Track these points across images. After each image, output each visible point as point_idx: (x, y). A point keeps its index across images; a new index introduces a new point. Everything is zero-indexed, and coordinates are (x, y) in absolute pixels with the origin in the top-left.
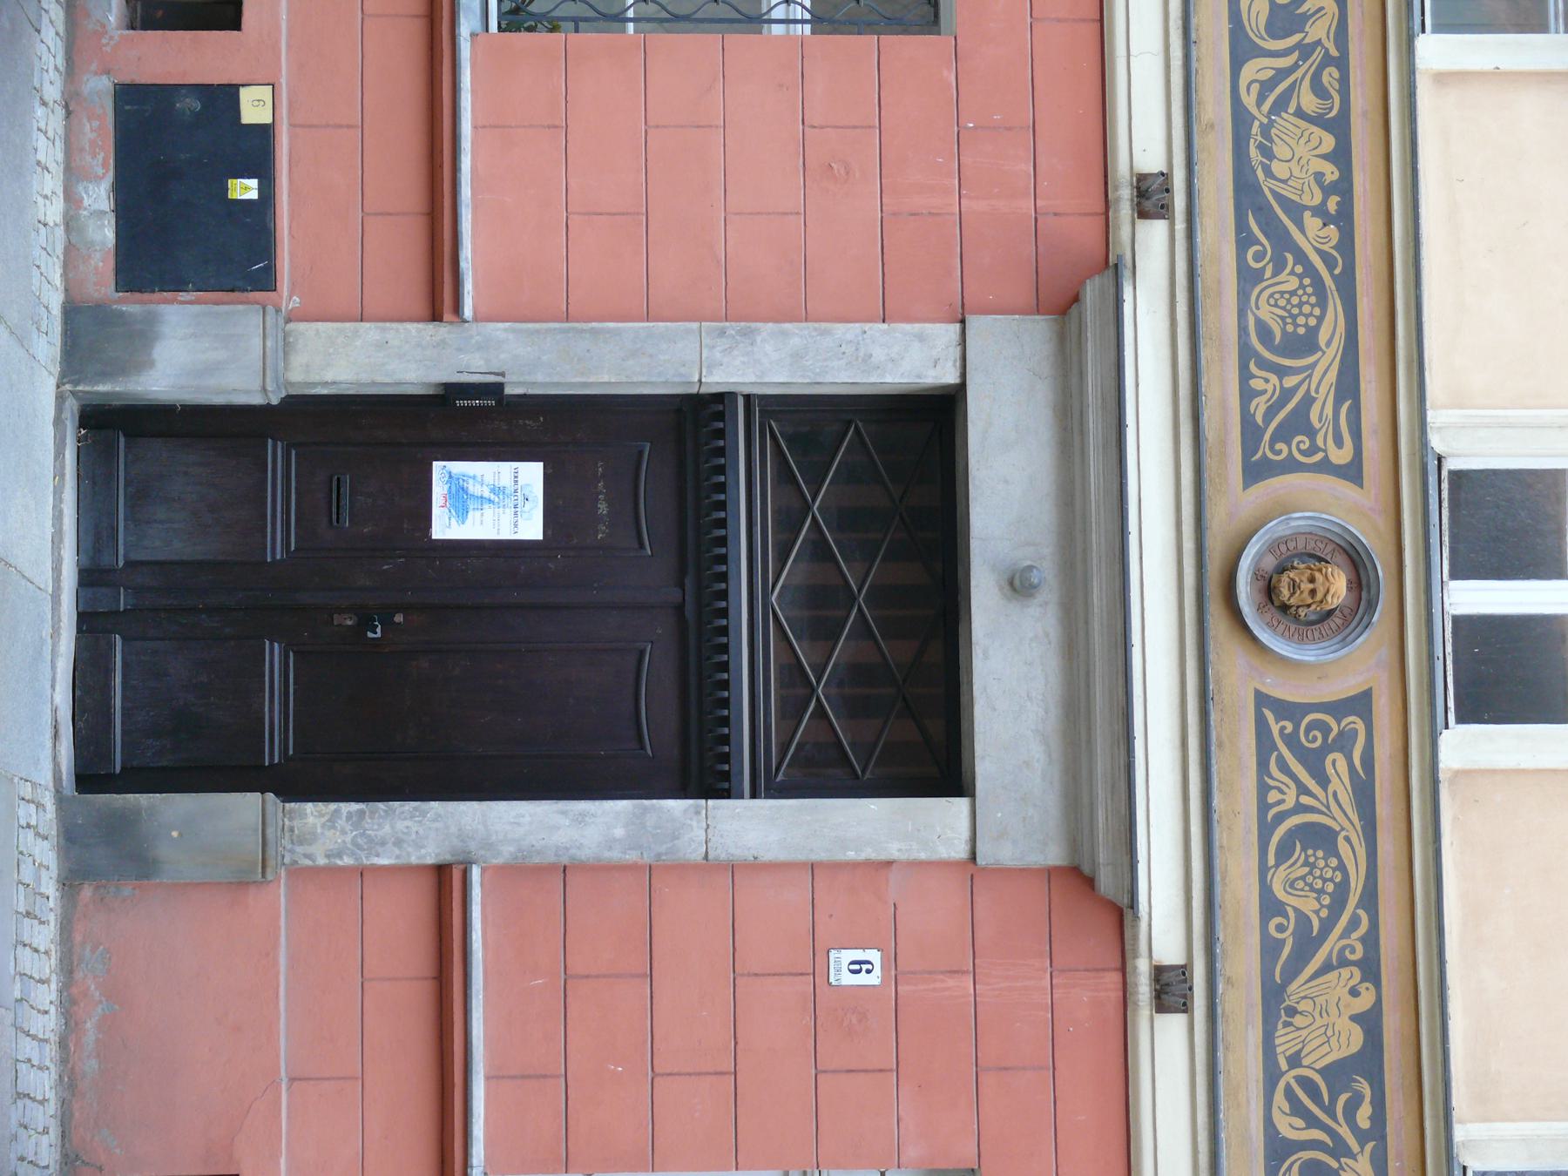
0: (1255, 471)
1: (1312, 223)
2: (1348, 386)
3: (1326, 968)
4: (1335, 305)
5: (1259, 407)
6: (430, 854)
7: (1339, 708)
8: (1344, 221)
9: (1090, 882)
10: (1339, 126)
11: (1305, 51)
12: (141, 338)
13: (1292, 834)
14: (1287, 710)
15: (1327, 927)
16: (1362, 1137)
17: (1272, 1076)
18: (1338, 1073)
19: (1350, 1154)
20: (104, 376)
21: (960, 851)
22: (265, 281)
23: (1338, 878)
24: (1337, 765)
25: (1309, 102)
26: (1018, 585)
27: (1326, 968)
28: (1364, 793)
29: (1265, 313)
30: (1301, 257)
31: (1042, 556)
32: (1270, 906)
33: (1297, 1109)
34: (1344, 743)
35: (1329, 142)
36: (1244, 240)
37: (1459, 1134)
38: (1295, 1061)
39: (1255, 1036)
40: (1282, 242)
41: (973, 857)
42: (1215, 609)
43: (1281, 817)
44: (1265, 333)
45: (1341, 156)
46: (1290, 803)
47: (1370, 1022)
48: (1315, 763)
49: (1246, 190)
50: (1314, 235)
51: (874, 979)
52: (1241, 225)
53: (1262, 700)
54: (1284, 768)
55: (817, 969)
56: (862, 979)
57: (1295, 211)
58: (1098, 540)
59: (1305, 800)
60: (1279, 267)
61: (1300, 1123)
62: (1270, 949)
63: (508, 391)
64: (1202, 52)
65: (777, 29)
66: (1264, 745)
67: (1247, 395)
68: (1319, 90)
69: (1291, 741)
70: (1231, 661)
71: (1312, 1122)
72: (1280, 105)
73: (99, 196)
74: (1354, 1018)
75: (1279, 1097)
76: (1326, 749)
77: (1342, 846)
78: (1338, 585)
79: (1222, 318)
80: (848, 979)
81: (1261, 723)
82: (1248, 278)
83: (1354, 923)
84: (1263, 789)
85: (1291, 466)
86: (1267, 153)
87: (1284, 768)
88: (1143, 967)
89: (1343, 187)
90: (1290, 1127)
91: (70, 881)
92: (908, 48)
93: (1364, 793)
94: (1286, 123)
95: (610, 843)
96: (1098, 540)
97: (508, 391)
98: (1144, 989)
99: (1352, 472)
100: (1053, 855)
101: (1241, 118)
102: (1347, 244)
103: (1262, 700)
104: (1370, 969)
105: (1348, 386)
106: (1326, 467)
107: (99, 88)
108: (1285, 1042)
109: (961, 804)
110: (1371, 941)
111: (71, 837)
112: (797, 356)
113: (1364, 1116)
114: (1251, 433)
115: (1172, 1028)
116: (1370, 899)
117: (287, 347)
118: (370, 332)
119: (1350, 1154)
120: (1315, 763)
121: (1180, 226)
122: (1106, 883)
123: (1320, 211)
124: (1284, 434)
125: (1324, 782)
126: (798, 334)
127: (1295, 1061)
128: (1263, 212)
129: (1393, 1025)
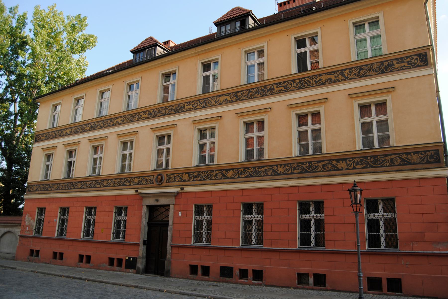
0: (153, 183)
1: (140, 179)
2: (149, 176)
3: (182, 177)
4: (144, 178)
5: (150, 183)
6: (170, 248)
7: (167, 176)
8: (140, 177)
9: (176, 195)
10: (135, 177)
11: (131, 180)
12: (139, 268)
13: (174, 180)
14: (167, 181)
15: (180, 177)
16: (193, 174)
17: (189, 181)
18: (189, 176)
19: (428, 155)
20: (140, 271)
21: (173, 205)
22: (136, 258)
23: (398, 157)
24: (170, 176)
25: (133, 180)
26: (157, 201)
27: (182, 177)
28: (172, 174)
29: (144, 183)
30: (141, 180)
31: (154, 199)
32: (178, 181)
33: (191, 179)
34: (169, 176)
35: (136, 178)
36: (140, 184)
37: (193, 166)
38: (188, 179)
39: (186, 182)
40: (141, 181)
41: (174, 204)
42: (161, 185)
43: (264, 174)
44: (145, 183)
45: (136, 177)
46: (320, 169)
47: (186, 173)
48: (170, 178)
49: (138, 184)
50: (140, 179)
51: (181, 212)
52: (139, 185)
53: (166, 182)
54: (384, 164)
55: (180, 217)
56: (181, 213)
57: (139, 180)
58: (154, 195)
59: (388, 162)
60: (142, 182)
61: (351, 166)
62: (181, 181)
63: (146, 239)
64: (91, 190)
65: (324, 217)
66: (169, 182)
67: (149, 184)
68: (133, 179)
69: (169, 180)
70: (165, 184)
71: (192, 178)
72: (133, 182)
73: (131, 270)
74: (414, 155)
75: (235, 177)
76: (169, 177)
77: (217, 173)
78: (160, 177)
79: (144, 186)
80: (181, 215)
81: (168, 182)
82: (142, 184)
83: (180, 175)
84: (172, 182)
85: (153, 180)
86: (136, 183)
87: (384, 164)
88: (181, 191)
89: (138, 177)
90: (192, 179)
91: (170, 277)
92: (325, 205)
93: (172, 174)
94: (134, 181)
95: (171, 233)
96: (154, 195)
97: (146, 239)
98: (182, 191)
99: (154, 176)
100: (174, 198)
101: (134, 185)
102: (83, 182)
103: (166, 182)
104: (183, 173)
105: (149, 176)
106: (153, 178)
107: (125, 270)
108: (187, 180)
109: (170, 205)
110: (181, 173)
111: (167, 277)
112: (144, 218)
113: (192, 174)
114: (151, 184)
115: (185, 189)
116: (178, 174)
117: (140, 257)
118: (140, 250)
119: (428, 155)
120: (170, 178)
121: (138, 189)
122: (176, 194)
123: (139, 179)
124: (151, 181)
125: (171, 177)
126: (142, 218)
127: (188, 179)
128: (139, 183)
129: (186, 172)
